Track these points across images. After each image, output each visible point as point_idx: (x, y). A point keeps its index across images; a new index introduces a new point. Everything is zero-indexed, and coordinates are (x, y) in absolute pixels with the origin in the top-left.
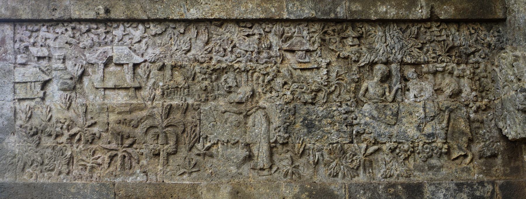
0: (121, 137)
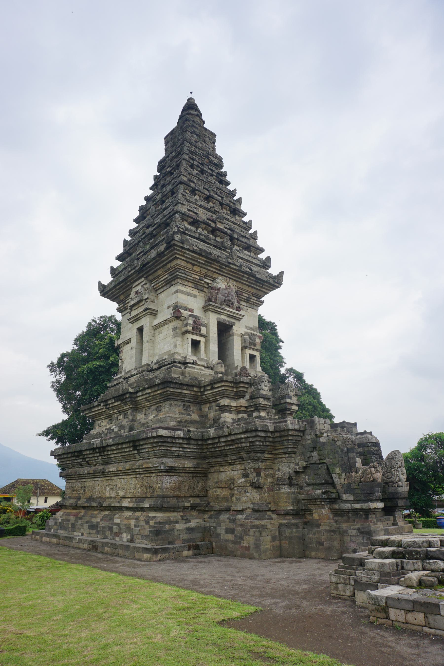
0: (174, 489)
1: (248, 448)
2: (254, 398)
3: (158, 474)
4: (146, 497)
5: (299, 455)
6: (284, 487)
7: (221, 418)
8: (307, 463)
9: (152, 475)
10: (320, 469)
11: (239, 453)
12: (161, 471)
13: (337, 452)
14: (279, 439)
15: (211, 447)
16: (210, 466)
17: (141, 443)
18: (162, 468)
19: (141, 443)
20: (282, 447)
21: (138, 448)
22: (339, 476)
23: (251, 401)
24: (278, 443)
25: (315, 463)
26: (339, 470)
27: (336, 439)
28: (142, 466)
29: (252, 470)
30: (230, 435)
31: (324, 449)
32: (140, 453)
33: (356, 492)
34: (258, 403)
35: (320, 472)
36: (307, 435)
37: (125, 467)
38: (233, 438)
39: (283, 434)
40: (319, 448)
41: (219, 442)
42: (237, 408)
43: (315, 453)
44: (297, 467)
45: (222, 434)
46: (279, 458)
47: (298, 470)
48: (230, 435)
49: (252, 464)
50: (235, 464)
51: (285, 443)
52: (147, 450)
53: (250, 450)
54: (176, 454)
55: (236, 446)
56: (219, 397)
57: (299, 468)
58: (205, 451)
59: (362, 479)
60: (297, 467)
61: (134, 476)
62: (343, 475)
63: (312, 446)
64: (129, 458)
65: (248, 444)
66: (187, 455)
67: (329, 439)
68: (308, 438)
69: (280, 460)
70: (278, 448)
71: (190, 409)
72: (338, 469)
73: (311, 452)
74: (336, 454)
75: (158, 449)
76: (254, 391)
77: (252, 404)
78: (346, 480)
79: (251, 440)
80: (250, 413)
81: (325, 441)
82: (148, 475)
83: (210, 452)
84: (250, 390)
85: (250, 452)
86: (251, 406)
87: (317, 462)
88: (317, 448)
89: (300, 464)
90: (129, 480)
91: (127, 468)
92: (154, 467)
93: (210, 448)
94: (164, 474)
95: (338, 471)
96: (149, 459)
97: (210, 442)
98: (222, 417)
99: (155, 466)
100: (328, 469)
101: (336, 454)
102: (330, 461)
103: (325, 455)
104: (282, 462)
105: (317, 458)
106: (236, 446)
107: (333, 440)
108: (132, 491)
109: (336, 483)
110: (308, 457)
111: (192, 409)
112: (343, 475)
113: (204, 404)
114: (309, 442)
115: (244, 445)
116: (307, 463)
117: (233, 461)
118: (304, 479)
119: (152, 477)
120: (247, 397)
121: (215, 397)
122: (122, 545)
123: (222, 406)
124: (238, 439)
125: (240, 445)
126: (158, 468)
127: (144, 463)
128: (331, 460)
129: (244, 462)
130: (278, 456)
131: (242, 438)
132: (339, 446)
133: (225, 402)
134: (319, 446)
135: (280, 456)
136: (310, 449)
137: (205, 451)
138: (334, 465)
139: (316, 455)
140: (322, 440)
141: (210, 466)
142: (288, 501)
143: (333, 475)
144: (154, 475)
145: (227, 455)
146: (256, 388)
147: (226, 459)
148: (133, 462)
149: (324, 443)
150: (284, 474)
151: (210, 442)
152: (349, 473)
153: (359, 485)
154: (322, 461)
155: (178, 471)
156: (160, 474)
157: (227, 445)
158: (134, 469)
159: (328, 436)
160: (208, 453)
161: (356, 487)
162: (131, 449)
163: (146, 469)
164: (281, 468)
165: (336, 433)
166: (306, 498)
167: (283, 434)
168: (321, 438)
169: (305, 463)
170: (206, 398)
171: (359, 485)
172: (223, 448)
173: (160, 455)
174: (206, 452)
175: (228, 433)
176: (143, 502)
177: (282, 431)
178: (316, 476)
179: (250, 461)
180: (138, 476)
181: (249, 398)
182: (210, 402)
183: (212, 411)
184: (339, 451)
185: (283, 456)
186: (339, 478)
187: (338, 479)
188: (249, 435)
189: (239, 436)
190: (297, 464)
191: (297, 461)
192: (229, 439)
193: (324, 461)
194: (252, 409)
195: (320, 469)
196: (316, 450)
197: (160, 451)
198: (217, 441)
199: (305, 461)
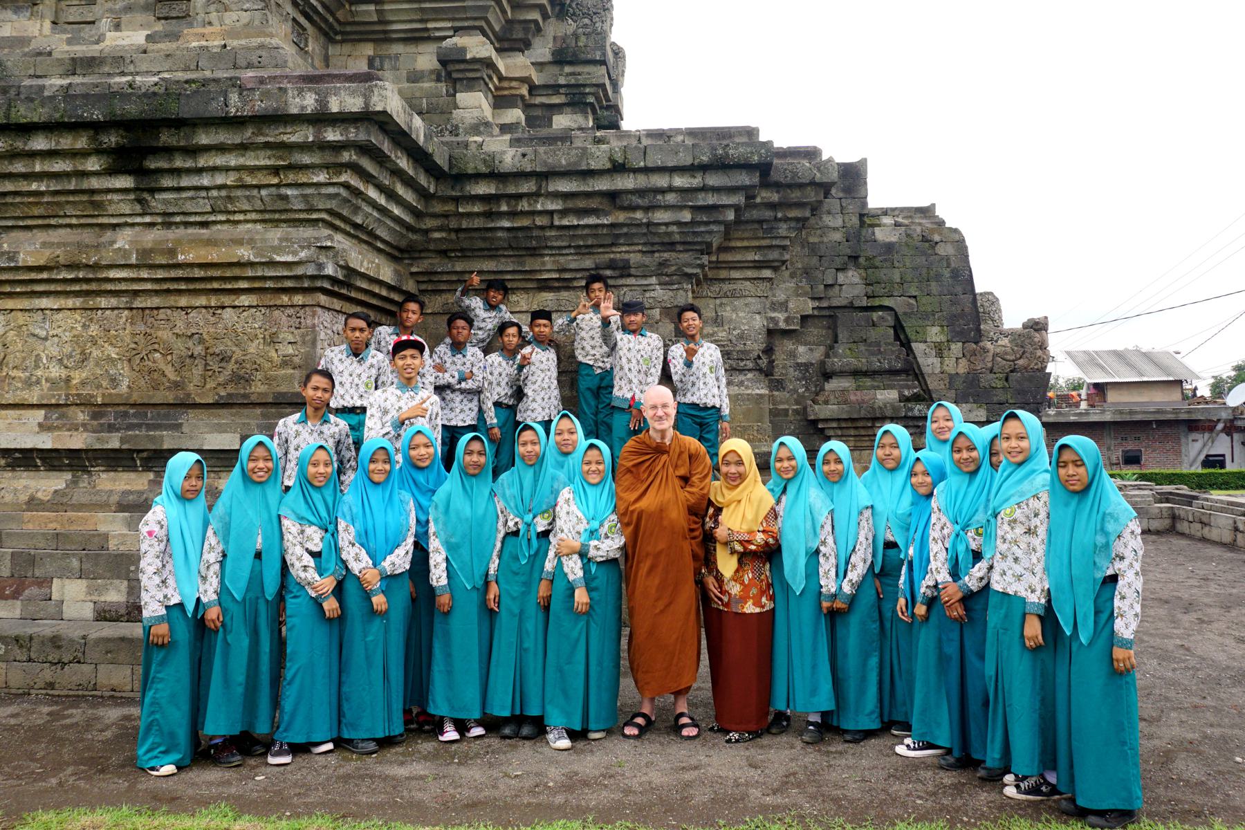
1: (674, 228)
2: (571, 63)
3: (285, 299)
4: (187, 405)
5: (792, 276)
6: (742, 377)
7: (456, 107)
8: (817, 304)
9: (227, 300)
10: (874, 325)
11: (613, 245)
12: (310, 285)
13: (938, 277)
14: (768, 214)
15: (476, 209)
16: (423, 287)
17: (204, 139)
18: (330, 270)
19: (204, 139)
20: (756, 243)
21: (153, 164)
22: (940, 351)
23: (555, 69)
24: (749, 227)
25: (851, 307)
26: (942, 332)
27: (937, 238)
28: (172, 252)
29: (656, 313)
30: (619, 168)
31: (888, 264)
32: (152, 191)
33: (995, 399)
34: (594, 81)
35: (873, 334)
36: (829, 213)
37: (12, 256)
38: (626, 182)
39: (795, 195)
40: (868, 259)
41: (535, 195)
42: (505, 84)
43: (850, 273)
44: (781, 316)
45: (575, 163)
46: (723, 280)
47: (782, 325)
48: (619, 168)
49: (659, 293)
50: (568, 288)
51: (783, 229)
52: (220, 179)
53: (677, 238)
54: (359, 220)
55: (621, 217)
56: (449, 25)
57: (787, 320)
58: (429, 223)
59: (1021, 362)
60: (781, 316)
61: (78, 302)
62: (953, 346)
63: (849, 252)
64: (18, 213)
65: (686, 216)
66: (378, 232)
67: (908, 235)
68: (831, 224)
69: (726, 287)
70: (739, 244)
71: (306, 45)
72: (936, 329)
73: (837, 270)
74: (933, 284)
75: (322, 177)
76: (576, 36)
77: (562, 81)
78: (963, 362)
79: (711, 199)
80: (538, 112)
81: (893, 239)
82: (202, 301)
83: (450, 230)
84: (554, 29)
85: (671, 246)
86: (555, 88)
87: (857, 303)
88: (862, 260)
89: (791, 305)
90: (21, 318)
91: (25, 259)
92: (272, 264)
93: (469, 215)
94: (323, 299)
95: (935, 333)
96: (204, 224)
97: (482, 189)
98: (461, 105)
99: (278, 259)
100: (898, 328)
101: (933, 284)
102: (909, 304)
103: (891, 282)
104: (734, 295)
105: (860, 290)
106: (621, 217)
107: (925, 239)
108: (56, 372)
109: (926, 370)
110: (826, 286)
111: (310, 48)
112: (953, 346)
113: (342, 42)
114: (837, 236)
115: (661, 216)
116: (817, 304)
117: (567, 276)
118: (793, 355)
119: (228, 314)
120: (542, 50)
121: (426, 21)
122: (122, 639)
123: (475, 60)
124: (640, 192)
125: (639, 215)
126: (299, 271)
127: (178, 242)
128: (912, 301)
129: (621, 282)
130: (723, 274)
131: (670, 189)
132: (948, 259)
133: (477, 46)
134: (870, 253)
135: (735, 274)
136: (838, 262)
137: (429, 223)
138: (925, 316)
139: (857, 280)
140: (880, 235)
141: (423, 287)
142: (755, 425)
143: (918, 348)
144: (245, 300)
145: (534, 252)
146: (586, 26)
147: (531, 264)
148: (62, 231)
149: (889, 247)
150: (741, 337)
151: (482, 189)
152: (976, 343)
153: (1007, 380)
154: (877, 302)
155: (353, 295)
156: (299, 299)
157: (564, 213)
158: (96, 267)
159: (897, 225)
160: (437, 235)
161: (999, 384)
162: (93, 164)
163: (198, 273)
164: (727, 313)
165: (926, 217)
166: (845, 416)
167: (795, 195)
168: (877, 230)
169: (811, 304)
170: (375, 19)
171: (1007, 380)
172: (540, 221)
173: (311, 210)
174: (427, 232)
175: (611, 160)
176: (178, 427)
177: (789, 186)
178: (862, 347)
179: (654, 280)
180: (103, 302)
181: (548, 57)
182: (384, 38)
183: (387, 74)
184: (947, 273)
185: (750, 274)
186: (940, 354)
187: (937, 361)
188: (713, 180)
189: (661, 181)
190: (784, 306)
191: (781, 297)
192: (603, 185)
193: (887, 302)
194: (556, 100)
195: (874, 325)
196: (858, 266)
197: (331, 190)
198: (527, 187)
199: (813, 299)
